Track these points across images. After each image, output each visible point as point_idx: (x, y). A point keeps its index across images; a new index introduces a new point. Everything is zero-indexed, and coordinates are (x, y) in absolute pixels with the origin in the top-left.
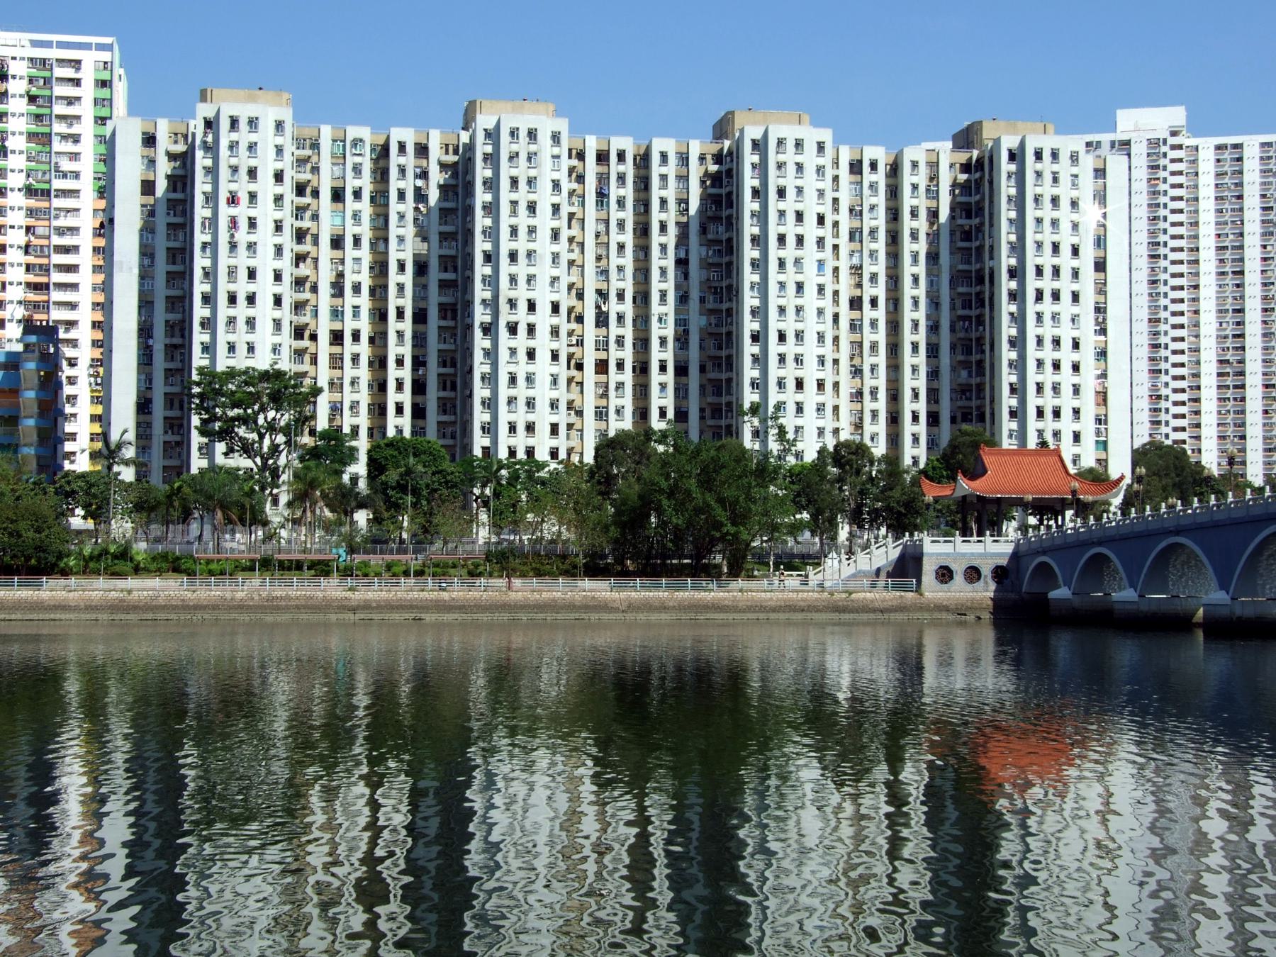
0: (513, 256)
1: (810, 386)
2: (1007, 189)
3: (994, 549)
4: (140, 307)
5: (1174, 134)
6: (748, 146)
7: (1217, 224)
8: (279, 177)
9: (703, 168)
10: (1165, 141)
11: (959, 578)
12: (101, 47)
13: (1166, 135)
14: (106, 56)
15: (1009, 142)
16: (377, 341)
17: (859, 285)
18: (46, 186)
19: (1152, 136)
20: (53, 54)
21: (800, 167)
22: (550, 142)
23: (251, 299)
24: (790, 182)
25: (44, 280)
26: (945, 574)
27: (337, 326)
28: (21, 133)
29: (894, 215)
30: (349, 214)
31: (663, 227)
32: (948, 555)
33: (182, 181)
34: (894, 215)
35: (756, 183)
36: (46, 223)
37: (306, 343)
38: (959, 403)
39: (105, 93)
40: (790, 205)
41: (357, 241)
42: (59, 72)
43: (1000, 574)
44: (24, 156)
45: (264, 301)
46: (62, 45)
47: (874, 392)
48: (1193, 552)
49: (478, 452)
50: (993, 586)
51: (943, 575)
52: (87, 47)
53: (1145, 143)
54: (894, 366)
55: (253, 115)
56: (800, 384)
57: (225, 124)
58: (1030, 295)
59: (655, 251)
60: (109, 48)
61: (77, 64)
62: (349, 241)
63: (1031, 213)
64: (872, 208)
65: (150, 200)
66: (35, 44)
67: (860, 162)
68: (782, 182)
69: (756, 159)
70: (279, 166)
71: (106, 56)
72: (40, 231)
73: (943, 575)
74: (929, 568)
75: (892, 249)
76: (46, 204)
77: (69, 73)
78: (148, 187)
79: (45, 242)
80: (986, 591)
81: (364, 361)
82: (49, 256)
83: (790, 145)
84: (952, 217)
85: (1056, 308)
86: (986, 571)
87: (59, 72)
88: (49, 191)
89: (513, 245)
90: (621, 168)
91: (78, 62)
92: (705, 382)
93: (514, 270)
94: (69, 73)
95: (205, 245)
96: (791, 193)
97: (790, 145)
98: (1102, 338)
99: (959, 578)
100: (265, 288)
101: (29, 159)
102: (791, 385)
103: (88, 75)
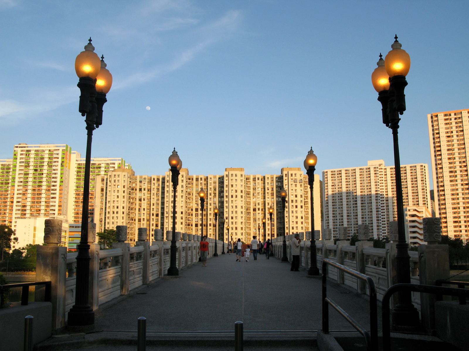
1: (239, 229)
4: (376, 248)
13: (378, 166)
17: (255, 205)
19: (375, 166)
20: (109, 162)
22: (113, 182)
23: (117, 213)
24: (234, 183)
27: (140, 218)
38: (279, 232)
40: (234, 188)
46: (111, 160)
53: (330, 172)
56: (236, 228)
61: (114, 164)
67: (255, 178)
68: (232, 183)
70: (124, 184)
77: (113, 166)
83: (234, 175)
87: (111, 166)
90: (201, 181)
94: (113, 166)
96: (234, 186)
97: (234, 175)
100: (120, 210)
102: (234, 229)
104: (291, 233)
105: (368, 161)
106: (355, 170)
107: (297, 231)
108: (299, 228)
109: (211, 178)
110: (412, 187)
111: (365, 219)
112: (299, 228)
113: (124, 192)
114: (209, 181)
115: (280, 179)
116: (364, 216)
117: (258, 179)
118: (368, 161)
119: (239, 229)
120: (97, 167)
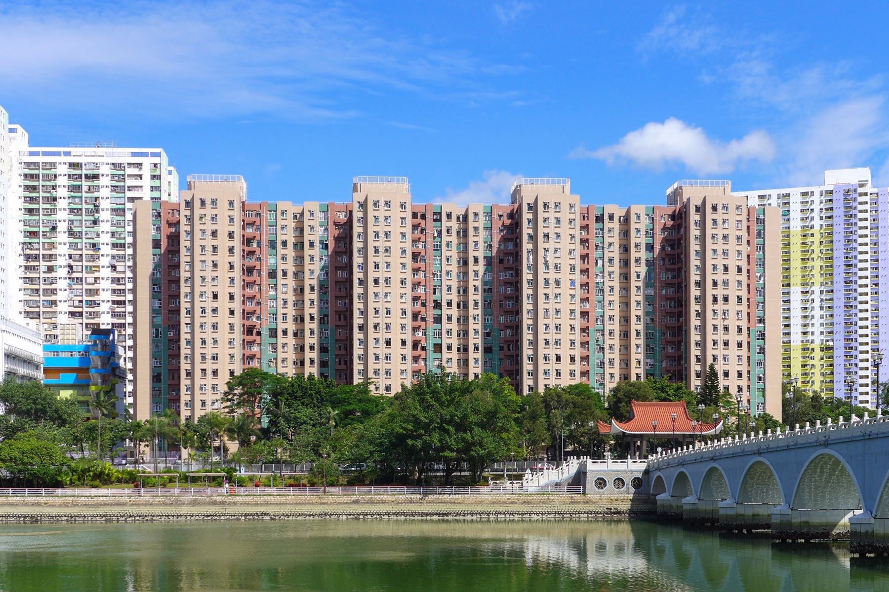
0: (376, 281)
1: (566, 359)
2: (694, 232)
3: (635, 466)
5: (861, 186)
6: (525, 208)
7: (802, 251)
8: (231, 235)
9: (501, 222)
10: (855, 190)
11: (610, 486)
12: (154, 155)
14: (156, 160)
15: (696, 201)
16: (299, 334)
18: (122, 241)
21: (558, 221)
25: (122, 298)
26: (601, 483)
28: (107, 210)
29: (625, 249)
30: (279, 257)
31: (476, 260)
32: (623, 472)
33: (174, 239)
34: (625, 249)
35: (531, 231)
36: (123, 264)
37: (419, 323)
39: (156, 183)
41: (285, 274)
42: (129, 171)
43: (638, 483)
44: (109, 223)
45: (224, 312)
47: (611, 362)
48: (768, 468)
49: (183, 421)
50: (633, 490)
51: (600, 484)
52: (145, 155)
54: (626, 348)
55: (214, 198)
57: (197, 204)
58: (709, 299)
59: (471, 275)
60: (158, 155)
61: (139, 165)
62: (280, 274)
63: (709, 246)
64: (610, 244)
65: (158, 251)
66: (134, 154)
69: (530, 216)
71: (156, 160)
72: (119, 269)
73: (600, 484)
74: (591, 480)
75: (623, 271)
76: (123, 253)
77: (135, 171)
78: (156, 244)
79: (122, 276)
80: (628, 493)
81: (454, 333)
82: (125, 284)
84: (663, 248)
85: (726, 307)
86: (628, 481)
87: (129, 171)
88: (124, 244)
89: (376, 275)
91: (141, 164)
92: (502, 357)
93: (376, 290)
94: (135, 171)
95: (186, 281)
98: (761, 325)
99: (610, 486)
101: (112, 225)
103: (146, 172)
104: (541, 390)
105: (826, 172)
106: (788, 195)
107: (558, 382)
108: (565, 374)
109: (476, 215)
110: (27, 268)
111: (810, 337)
112: (565, 374)
113: (231, 250)
114: (471, 224)
115: (515, 216)
116: (810, 329)
117: (449, 216)
118: (826, 172)
119: (566, 359)
120: (86, 175)
